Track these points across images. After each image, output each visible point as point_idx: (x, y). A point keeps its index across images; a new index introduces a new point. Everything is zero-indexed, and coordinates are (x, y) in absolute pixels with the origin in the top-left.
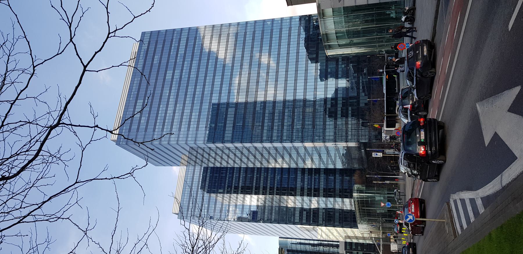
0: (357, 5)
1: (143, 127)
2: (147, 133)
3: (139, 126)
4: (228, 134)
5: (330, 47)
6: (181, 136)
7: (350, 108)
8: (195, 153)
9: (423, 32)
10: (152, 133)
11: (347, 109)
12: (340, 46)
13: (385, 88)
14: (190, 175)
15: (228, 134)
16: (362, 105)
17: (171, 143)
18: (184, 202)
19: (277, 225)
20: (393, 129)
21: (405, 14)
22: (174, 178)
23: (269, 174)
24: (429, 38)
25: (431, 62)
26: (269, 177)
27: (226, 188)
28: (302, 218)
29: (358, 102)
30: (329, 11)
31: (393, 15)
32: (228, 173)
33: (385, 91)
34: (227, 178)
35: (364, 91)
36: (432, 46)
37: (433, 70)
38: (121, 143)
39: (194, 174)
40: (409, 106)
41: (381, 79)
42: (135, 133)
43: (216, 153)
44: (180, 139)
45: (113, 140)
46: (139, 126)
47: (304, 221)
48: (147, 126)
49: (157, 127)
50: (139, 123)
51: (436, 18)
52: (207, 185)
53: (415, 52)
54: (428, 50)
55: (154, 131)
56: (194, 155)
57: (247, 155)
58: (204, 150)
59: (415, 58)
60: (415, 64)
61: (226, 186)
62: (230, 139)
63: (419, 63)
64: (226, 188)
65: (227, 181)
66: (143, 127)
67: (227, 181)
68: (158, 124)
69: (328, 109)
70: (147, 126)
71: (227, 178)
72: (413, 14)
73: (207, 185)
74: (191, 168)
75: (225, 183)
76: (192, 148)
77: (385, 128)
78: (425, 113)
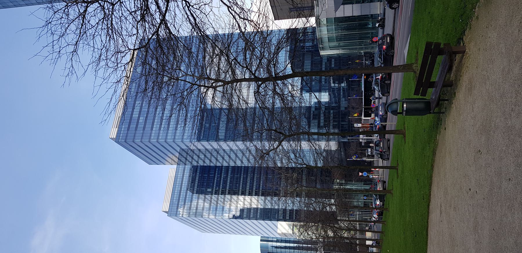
0: (351, 5)
1: (141, 126)
2: (145, 132)
3: (137, 125)
4: (222, 133)
5: (323, 49)
6: (177, 134)
7: (332, 111)
8: (185, 154)
9: (388, 30)
10: (150, 132)
11: (330, 112)
12: (331, 48)
13: (363, 86)
14: (180, 175)
15: (222, 133)
16: (342, 109)
17: (168, 141)
18: (174, 201)
19: (262, 222)
20: (369, 118)
21: (378, 22)
22: (166, 175)
23: (256, 175)
24: (391, 33)
25: (391, 45)
26: (255, 177)
27: (214, 188)
28: (286, 215)
29: (339, 107)
30: (324, 21)
31: (370, 26)
32: (216, 174)
33: (363, 90)
34: (216, 178)
35: (344, 97)
36: (392, 38)
37: (393, 51)
38: (120, 140)
39: (183, 175)
40: (379, 77)
41: (360, 81)
42: (134, 132)
43: (205, 156)
44: (177, 137)
45: (112, 139)
46: (137, 125)
47: (288, 218)
48: (145, 125)
49: (155, 126)
50: (138, 122)
51: (394, 21)
52: (196, 185)
53: (382, 41)
54: (390, 39)
55: (152, 129)
56: (184, 157)
57: (234, 159)
58: (193, 152)
59: (383, 44)
60: (382, 48)
61: (215, 185)
62: (223, 137)
63: (385, 47)
64: (214, 188)
65: (215, 181)
66: (141, 126)
67: (215, 181)
68: (155, 123)
69: (312, 112)
70: (145, 125)
71: (216, 178)
72: (384, 22)
73: (196, 185)
74: (181, 167)
75: (214, 183)
76: (183, 150)
77: (363, 118)
78: (389, 82)
